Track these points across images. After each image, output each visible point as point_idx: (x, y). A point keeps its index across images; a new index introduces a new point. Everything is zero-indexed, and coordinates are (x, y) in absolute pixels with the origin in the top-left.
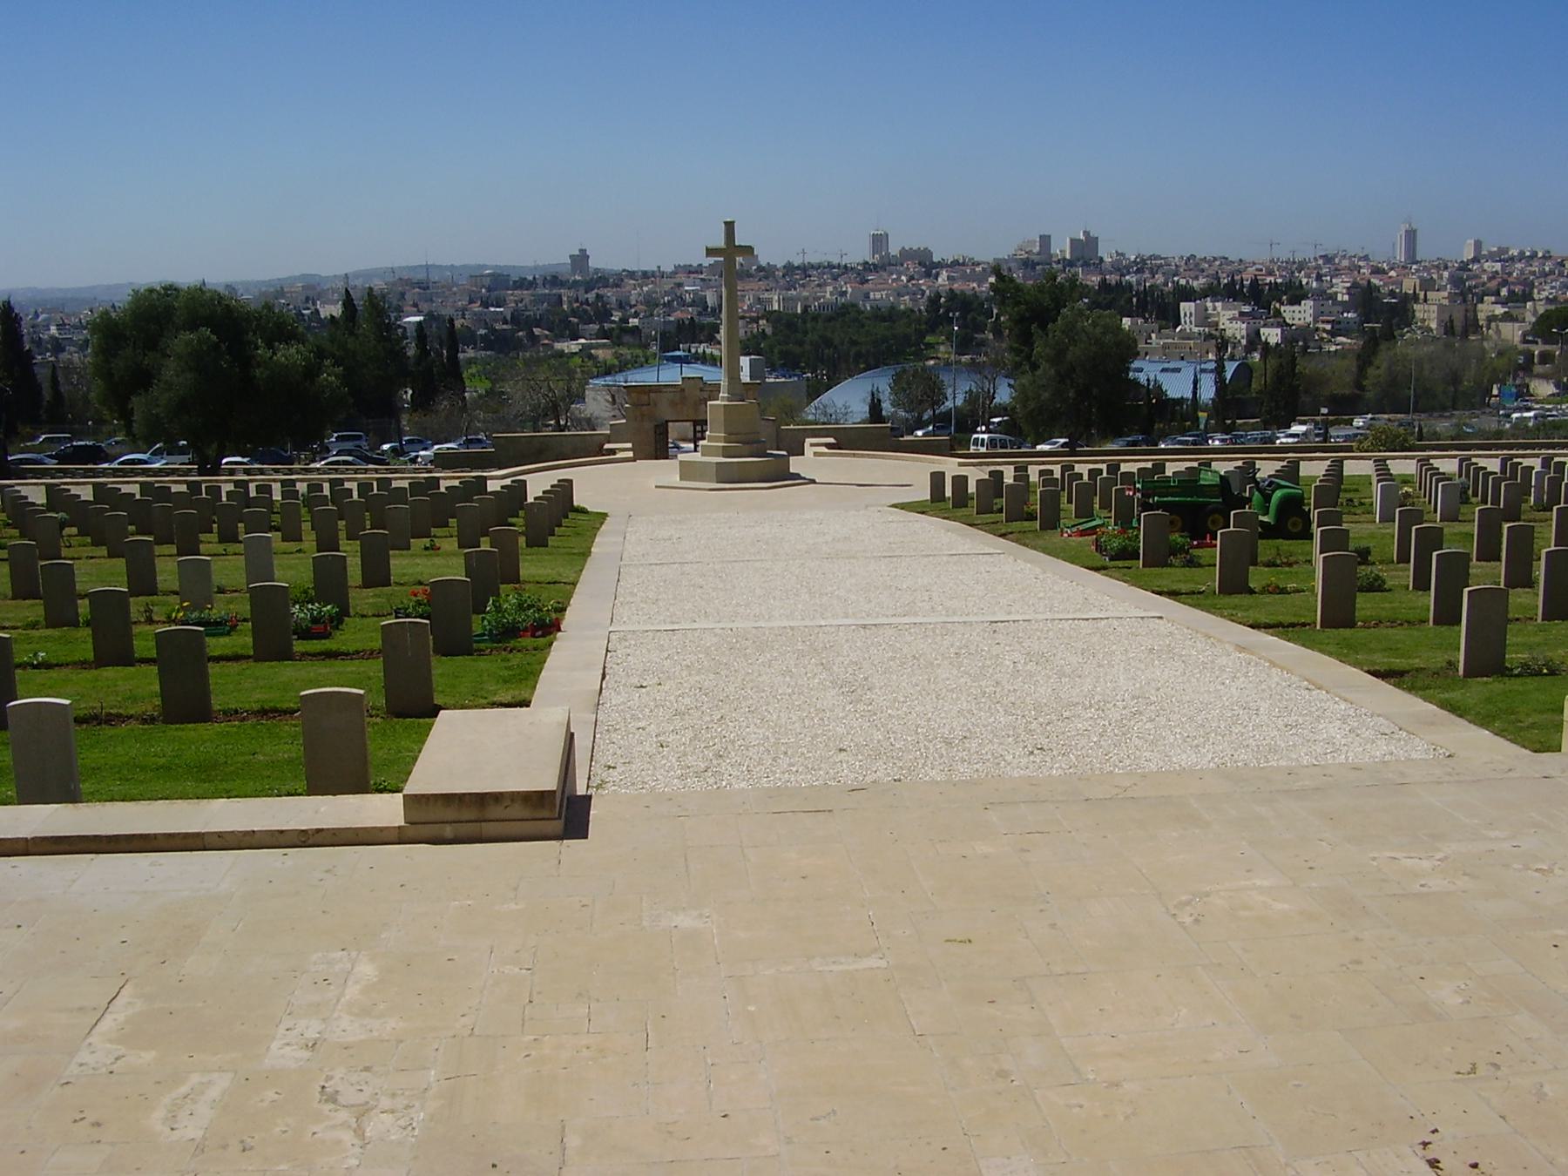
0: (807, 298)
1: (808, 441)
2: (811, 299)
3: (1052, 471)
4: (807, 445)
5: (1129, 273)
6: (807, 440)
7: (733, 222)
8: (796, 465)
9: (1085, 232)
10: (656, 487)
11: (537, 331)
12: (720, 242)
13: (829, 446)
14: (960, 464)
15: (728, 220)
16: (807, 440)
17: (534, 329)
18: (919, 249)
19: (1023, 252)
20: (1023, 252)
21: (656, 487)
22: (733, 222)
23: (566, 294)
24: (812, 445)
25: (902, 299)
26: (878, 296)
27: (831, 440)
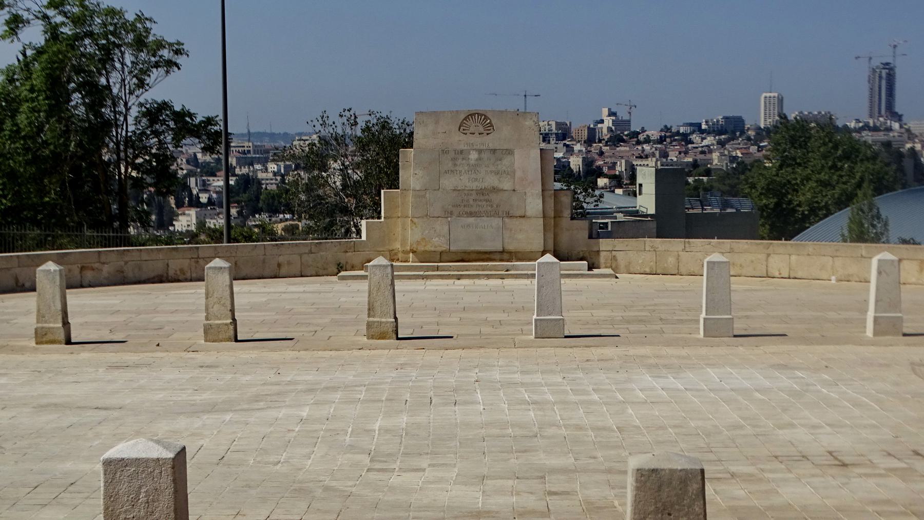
18: (820, 113)
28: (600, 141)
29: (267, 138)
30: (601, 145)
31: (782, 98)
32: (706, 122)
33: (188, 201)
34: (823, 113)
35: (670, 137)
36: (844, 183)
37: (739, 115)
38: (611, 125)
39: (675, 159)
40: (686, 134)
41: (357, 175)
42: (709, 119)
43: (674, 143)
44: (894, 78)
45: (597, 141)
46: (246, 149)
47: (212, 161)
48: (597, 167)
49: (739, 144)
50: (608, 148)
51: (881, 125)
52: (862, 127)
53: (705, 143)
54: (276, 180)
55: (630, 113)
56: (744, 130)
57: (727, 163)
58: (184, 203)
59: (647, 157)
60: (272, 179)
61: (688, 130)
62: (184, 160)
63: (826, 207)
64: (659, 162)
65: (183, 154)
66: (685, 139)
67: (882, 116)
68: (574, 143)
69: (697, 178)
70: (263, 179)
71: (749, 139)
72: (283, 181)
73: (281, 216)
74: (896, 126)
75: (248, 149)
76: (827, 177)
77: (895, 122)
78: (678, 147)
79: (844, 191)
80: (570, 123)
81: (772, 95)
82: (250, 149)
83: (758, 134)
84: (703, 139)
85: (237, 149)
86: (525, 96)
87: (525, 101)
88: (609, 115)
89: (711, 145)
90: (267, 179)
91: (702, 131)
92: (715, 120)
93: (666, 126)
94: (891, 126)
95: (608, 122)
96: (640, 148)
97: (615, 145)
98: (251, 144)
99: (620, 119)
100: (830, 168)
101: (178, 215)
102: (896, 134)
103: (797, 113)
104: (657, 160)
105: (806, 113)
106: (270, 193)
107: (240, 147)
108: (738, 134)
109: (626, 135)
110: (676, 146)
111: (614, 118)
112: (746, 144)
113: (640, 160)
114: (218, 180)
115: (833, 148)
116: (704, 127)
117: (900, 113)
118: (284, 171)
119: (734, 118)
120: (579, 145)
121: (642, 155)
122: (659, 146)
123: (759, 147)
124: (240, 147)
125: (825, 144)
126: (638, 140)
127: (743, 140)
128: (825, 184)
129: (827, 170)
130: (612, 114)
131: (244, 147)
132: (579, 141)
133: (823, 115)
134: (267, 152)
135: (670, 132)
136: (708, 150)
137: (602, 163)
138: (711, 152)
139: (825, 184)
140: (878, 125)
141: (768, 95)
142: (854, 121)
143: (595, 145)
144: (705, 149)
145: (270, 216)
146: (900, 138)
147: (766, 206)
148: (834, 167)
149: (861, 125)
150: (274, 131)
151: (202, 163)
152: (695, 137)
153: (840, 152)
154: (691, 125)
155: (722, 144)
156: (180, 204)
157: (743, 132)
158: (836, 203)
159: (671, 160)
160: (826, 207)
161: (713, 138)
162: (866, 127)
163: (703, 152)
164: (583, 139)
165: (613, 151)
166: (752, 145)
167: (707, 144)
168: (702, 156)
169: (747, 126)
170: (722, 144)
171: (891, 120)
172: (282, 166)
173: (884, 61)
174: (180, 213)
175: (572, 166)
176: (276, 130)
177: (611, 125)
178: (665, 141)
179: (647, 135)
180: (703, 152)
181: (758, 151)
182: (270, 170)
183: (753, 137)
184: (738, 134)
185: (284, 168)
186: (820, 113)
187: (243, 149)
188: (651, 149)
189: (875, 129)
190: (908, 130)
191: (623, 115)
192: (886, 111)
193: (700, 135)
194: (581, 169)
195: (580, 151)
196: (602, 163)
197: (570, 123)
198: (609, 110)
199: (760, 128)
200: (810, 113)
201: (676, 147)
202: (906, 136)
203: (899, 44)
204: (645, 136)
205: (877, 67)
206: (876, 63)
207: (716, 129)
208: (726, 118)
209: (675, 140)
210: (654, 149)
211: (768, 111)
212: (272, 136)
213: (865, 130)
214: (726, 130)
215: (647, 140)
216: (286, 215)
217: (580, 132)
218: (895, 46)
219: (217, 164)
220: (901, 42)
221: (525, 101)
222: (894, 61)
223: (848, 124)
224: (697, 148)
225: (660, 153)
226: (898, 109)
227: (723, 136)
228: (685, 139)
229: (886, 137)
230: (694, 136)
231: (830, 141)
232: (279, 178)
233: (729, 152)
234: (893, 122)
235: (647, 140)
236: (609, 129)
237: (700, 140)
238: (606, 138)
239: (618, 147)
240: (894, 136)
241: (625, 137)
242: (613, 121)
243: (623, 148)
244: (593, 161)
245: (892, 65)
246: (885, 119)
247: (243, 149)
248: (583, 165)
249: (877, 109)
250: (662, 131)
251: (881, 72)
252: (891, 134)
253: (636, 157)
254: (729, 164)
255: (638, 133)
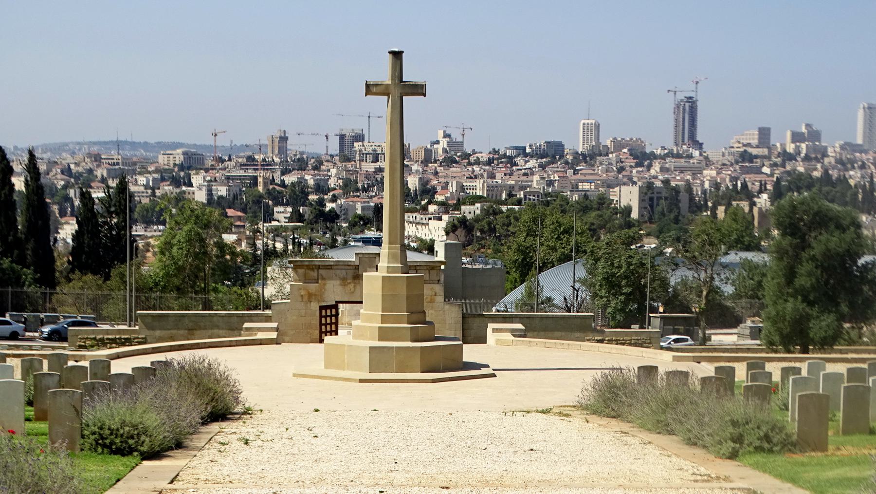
0: (512, 187)
1: (491, 326)
2: (516, 188)
3: (800, 369)
4: (489, 331)
5: (853, 168)
6: (489, 325)
7: (402, 52)
8: (470, 353)
9: (807, 126)
10: (294, 375)
11: (230, 212)
12: (385, 76)
13: (515, 333)
14: (675, 358)
15: (396, 50)
16: (489, 325)
17: (227, 210)
18: (631, 139)
19: (741, 145)
20: (741, 145)
21: (294, 375)
22: (402, 52)
23: (261, 175)
24: (495, 330)
25: (611, 190)
26: (586, 186)
27: (520, 326)
28: (435, 162)
29: (127, 146)
30: (436, 165)
31: (599, 125)
32: (530, 146)
33: (71, 212)
34: (634, 139)
35: (498, 159)
36: (563, 248)
37: (557, 139)
38: (445, 146)
39: (500, 182)
40: (511, 157)
41: (222, 191)
42: (532, 143)
43: (501, 165)
44: (697, 111)
45: (432, 161)
46: (115, 161)
47: (84, 172)
48: (431, 186)
49: (558, 167)
50: (442, 168)
51: (683, 153)
52: (667, 153)
53: (528, 165)
54: (147, 193)
55: (463, 135)
56: (563, 153)
57: (544, 187)
58: (66, 213)
59: (476, 177)
60: (143, 192)
61: (513, 153)
62: (59, 171)
63: (552, 262)
64: (485, 184)
65: (58, 164)
66: (511, 161)
67: (685, 144)
68: (412, 163)
69: (509, 207)
70: (135, 192)
71: (567, 163)
72: (154, 194)
73: (155, 227)
74: (696, 153)
75: (117, 161)
76: (553, 244)
77: (696, 150)
78: (504, 169)
79: (563, 254)
80: (409, 144)
81: (590, 122)
82: (119, 161)
83: (575, 158)
84: (526, 162)
85: (107, 161)
86: (369, 117)
87: (369, 121)
88: (444, 137)
89: (533, 168)
90: (139, 192)
91: (526, 155)
92: (538, 144)
93: (494, 149)
94: (692, 154)
95: (444, 143)
96: (470, 169)
97: (448, 166)
98: (120, 157)
99: (454, 140)
100: (556, 238)
101: (62, 224)
102: (695, 161)
103: (611, 139)
104: (484, 182)
105: (620, 139)
106: (144, 206)
107: (110, 159)
108: (557, 157)
109: (459, 157)
110: (502, 168)
111: (448, 140)
112: (564, 168)
113: (470, 180)
114: (99, 192)
115: (558, 226)
116: (528, 150)
117: (700, 142)
118: (153, 184)
119: (554, 143)
120: (416, 165)
121: (472, 176)
122: (487, 167)
123: (575, 170)
124: (110, 159)
125: (553, 223)
126: (469, 161)
127: (561, 164)
128: (554, 249)
129: (554, 240)
130: (447, 135)
131: (113, 159)
132: (417, 161)
133: (634, 141)
134: (135, 164)
135: (498, 155)
136: (529, 173)
137: (437, 182)
138: (533, 174)
139: (554, 249)
140: (681, 152)
141: (586, 122)
142: (660, 148)
143: (430, 165)
144: (528, 171)
145: (145, 227)
146: (698, 165)
147: (518, 260)
148: (558, 238)
149: (666, 151)
150: (134, 140)
151: (75, 174)
152: (520, 160)
153: (562, 229)
154: (516, 148)
155: (543, 167)
156: (63, 213)
157: (562, 156)
158: (558, 261)
159: (496, 182)
160: (552, 262)
161: (535, 161)
162: (671, 154)
163: (525, 175)
164: (420, 159)
165: (447, 172)
166: (569, 169)
167: (529, 166)
168: (525, 178)
169: (566, 151)
170: (543, 167)
171: (693, 148)
172: (151, 179)
173: (688, 95)
174: (63, 221)
175: (410, 186)
176: (136, 140)
177: (445, 146)
178: (493, 163)
179: (477, 157)
180: (525, 175)
181: (574, 174)
182: (139, 183)
183: (570, 161)
184: (557, 157)
185: (153, 181)
186: (631, 139)
187: (112, 161)
188: (480, 170)
189: (678, 156)
190: (707, 158)
191: (457, 136)
192: (689, 140)
193: (524, 158)
194: (417, 188)
195: (417, 171)
196: (437, 182)
197: (409, 144)
198: (445, 132)
199: (577, 153)
200: (623, 139)
201: (502, 169)
202: (704, 163)
203: (700, 80)
204: (475, 158)
205: (682, 101)
206: (681, 96)
207: (538, 153)
208: (547, 143)
209: (502, 162)
210: (482, 171)
211: (586, 136)
212: (134, 145)
213: (669, 157)
214: (547, 154)
215: (478, 162)
216: (159, 227)
217: (417, 152)
218: (697, 83)
219: (89, 174)
220: (703, 79)
221: (369, 121)
222: (696, 95)
223: (655, 151)
224: (521, 170)
225: (487, 174)
226: (699, 138)
227: (545, 159)
228: (511, 161)
229: (686, 164)
230: (519, 159)
231: (557, 222)
232: (150, 191)
233: (548, 175)
234: (694, 150)
235: (478, 162)
236: (445, 151)
237: (524, 162)
238: (441, 159)
239: (451, 167)
240: (694, 163)
241: (457, 159)
242: (448, 142)
243: (455, 170)
244: (428, 181)
245: (694, 99)
246: (687, 147)
247: (112, 161)
248: (419, 184)
249: (681, 137)
250: (490, 153)
251: (684, 105)
252: (691, 161)
253: (467, 178)
254: (546, 187)
255: (470, 155)
